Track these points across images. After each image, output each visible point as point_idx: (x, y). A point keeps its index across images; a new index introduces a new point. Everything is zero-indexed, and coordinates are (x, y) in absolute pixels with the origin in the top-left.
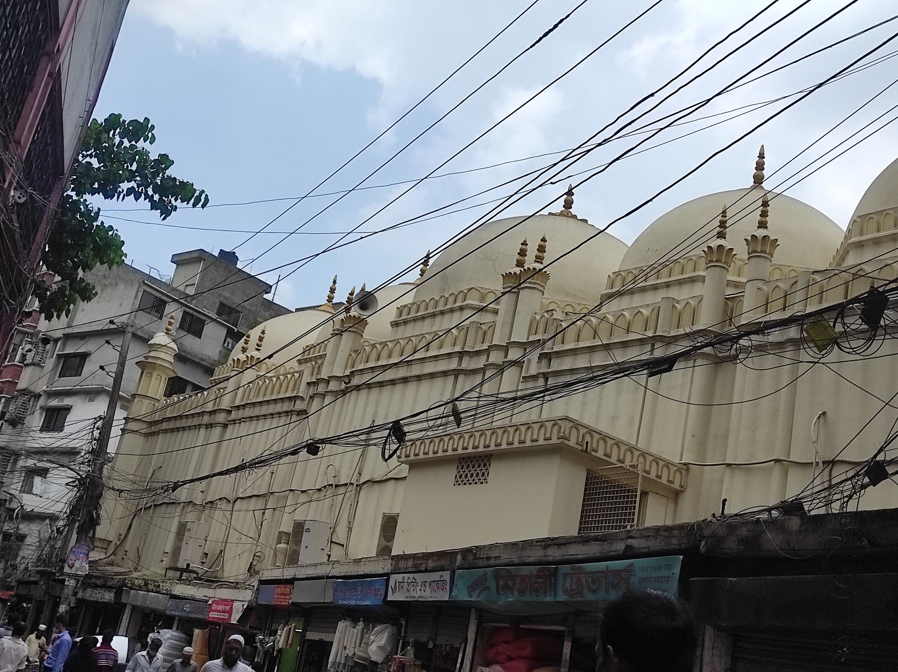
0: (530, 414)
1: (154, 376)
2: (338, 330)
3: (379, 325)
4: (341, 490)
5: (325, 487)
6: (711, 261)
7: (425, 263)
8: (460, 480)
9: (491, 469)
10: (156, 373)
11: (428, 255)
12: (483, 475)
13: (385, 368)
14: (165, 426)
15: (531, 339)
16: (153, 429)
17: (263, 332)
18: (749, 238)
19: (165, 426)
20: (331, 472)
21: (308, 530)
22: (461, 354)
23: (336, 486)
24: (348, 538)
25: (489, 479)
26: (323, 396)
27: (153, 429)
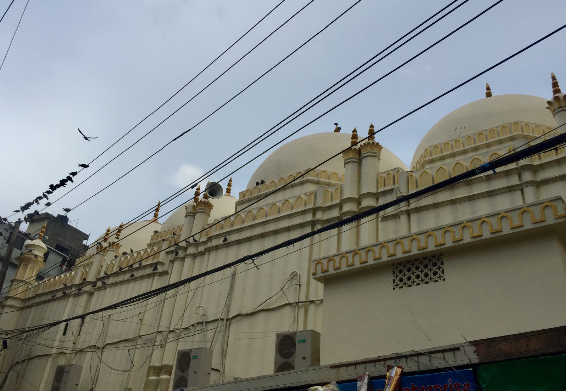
0: (104, 332)
1: (29, 267)
2: (190, 213)
3: (223, 207)
4: (210, 326)
5: (193, 325)
6: (555, 110)
7: (157, 210)
8: (399, 283)
9: (446, 267)
10: (30, 265)
11: (159, 205)
12: (435, 273)
13: (240, 230)
14: (37, 300)
15: (381, 190)
16: (27, 304)
17: (230, 181)
18: (547, 105)
19: (37, 300)
20: (201, 311)
21: (195, 357)
22: (314, 210)
23: (206, 322)
24: (223, 364)
25: (446, 276)
26: (183, 259)
27: (27, 304)
